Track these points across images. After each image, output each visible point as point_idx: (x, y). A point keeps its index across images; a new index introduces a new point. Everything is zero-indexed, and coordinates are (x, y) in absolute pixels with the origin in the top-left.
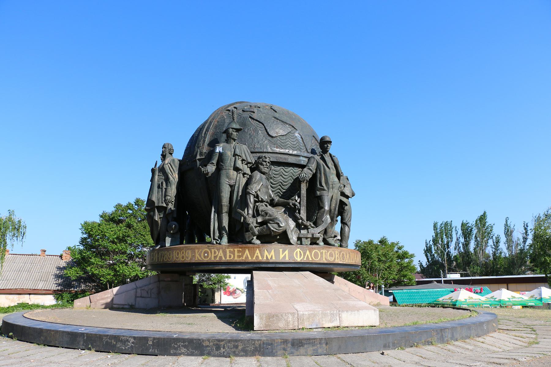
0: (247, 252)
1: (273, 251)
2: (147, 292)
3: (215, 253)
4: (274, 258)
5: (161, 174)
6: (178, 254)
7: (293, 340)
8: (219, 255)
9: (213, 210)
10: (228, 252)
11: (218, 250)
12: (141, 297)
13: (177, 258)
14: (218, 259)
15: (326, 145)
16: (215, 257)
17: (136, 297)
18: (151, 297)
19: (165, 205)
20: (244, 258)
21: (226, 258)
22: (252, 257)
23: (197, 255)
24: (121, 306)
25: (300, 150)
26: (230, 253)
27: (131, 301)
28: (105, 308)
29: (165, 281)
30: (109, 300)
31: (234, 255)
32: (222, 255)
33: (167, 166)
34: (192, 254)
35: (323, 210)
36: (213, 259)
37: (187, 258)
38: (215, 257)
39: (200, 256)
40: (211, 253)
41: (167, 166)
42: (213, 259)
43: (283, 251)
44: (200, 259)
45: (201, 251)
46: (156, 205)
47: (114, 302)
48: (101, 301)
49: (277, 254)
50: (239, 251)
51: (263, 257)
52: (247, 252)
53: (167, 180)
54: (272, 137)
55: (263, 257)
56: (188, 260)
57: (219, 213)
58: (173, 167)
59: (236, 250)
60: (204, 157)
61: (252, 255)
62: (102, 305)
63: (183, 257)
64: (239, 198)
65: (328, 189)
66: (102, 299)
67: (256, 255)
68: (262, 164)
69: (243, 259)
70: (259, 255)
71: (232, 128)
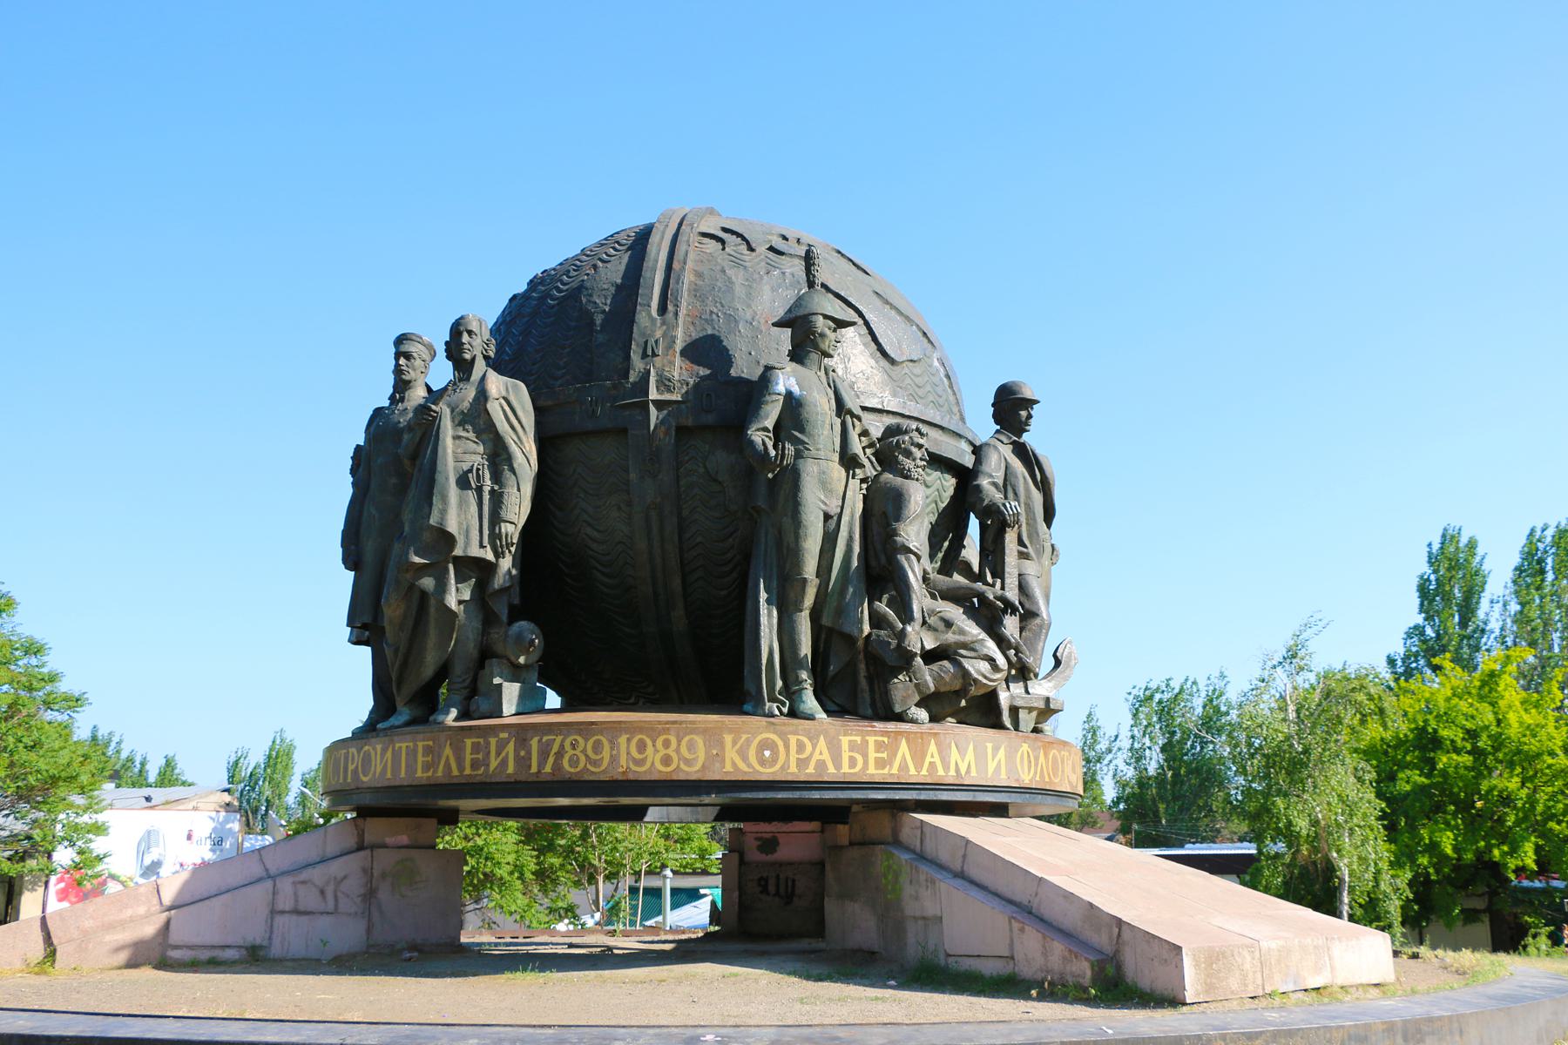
0: (904, 747)
1: (971, 747)
2: (322, 892)
3: (801, 747)
4: (974, 773)
5: (471, 435)
6: (642, 747)
7: (1405, 1022)
8: (816, 756)
9: (763, 596)
10: (845, 746)
11: (814, 740)
12: (297, 912)
14: (811, 770)
15: (1024, 413)
16: (802, 763)
17: (274, 912)
18: (335, 912)
19: (490, 556)
20: (895, 771)
21: (838, 766)
22: (919, 767)
23: (731, 754)
24: (205, 955)
25: (938, 406)
26: (851, 750)
27: (254, 933)
28: (132, 964)
29: (385, 846)
30: (149, 930)
31: (865, 756)
32: (826, 756)
33: (496, 404)
34: (708, 748)
35: (1038, 621)
36: (793, 768)
37: (688, 762)
38: (802, 763)
39: (745, 759)
40: (787, 747)
41: (496, 404)
42: (793, 768)
43: (996, 749)
44: (742, 766)
45: (748, 742)
46: (458, 552)
47: (175, 937)
48: (108, 938)
49: (981, 757)
50: (880, 747)
51: (946, 767)
52: (904, 747)
53: (499, 457)
54: (892, 362)
55: (946, 767)
58: (520, 413)
59: (871, 740)
60: (677, 397)
61: (919, 756)
62: (118, 949)
63: (666, 760)
64: (855, 563)
66: (110, 927)
67: (928, 759)
68: (908, 454)
69: (890, 773)
71: (826, 317)
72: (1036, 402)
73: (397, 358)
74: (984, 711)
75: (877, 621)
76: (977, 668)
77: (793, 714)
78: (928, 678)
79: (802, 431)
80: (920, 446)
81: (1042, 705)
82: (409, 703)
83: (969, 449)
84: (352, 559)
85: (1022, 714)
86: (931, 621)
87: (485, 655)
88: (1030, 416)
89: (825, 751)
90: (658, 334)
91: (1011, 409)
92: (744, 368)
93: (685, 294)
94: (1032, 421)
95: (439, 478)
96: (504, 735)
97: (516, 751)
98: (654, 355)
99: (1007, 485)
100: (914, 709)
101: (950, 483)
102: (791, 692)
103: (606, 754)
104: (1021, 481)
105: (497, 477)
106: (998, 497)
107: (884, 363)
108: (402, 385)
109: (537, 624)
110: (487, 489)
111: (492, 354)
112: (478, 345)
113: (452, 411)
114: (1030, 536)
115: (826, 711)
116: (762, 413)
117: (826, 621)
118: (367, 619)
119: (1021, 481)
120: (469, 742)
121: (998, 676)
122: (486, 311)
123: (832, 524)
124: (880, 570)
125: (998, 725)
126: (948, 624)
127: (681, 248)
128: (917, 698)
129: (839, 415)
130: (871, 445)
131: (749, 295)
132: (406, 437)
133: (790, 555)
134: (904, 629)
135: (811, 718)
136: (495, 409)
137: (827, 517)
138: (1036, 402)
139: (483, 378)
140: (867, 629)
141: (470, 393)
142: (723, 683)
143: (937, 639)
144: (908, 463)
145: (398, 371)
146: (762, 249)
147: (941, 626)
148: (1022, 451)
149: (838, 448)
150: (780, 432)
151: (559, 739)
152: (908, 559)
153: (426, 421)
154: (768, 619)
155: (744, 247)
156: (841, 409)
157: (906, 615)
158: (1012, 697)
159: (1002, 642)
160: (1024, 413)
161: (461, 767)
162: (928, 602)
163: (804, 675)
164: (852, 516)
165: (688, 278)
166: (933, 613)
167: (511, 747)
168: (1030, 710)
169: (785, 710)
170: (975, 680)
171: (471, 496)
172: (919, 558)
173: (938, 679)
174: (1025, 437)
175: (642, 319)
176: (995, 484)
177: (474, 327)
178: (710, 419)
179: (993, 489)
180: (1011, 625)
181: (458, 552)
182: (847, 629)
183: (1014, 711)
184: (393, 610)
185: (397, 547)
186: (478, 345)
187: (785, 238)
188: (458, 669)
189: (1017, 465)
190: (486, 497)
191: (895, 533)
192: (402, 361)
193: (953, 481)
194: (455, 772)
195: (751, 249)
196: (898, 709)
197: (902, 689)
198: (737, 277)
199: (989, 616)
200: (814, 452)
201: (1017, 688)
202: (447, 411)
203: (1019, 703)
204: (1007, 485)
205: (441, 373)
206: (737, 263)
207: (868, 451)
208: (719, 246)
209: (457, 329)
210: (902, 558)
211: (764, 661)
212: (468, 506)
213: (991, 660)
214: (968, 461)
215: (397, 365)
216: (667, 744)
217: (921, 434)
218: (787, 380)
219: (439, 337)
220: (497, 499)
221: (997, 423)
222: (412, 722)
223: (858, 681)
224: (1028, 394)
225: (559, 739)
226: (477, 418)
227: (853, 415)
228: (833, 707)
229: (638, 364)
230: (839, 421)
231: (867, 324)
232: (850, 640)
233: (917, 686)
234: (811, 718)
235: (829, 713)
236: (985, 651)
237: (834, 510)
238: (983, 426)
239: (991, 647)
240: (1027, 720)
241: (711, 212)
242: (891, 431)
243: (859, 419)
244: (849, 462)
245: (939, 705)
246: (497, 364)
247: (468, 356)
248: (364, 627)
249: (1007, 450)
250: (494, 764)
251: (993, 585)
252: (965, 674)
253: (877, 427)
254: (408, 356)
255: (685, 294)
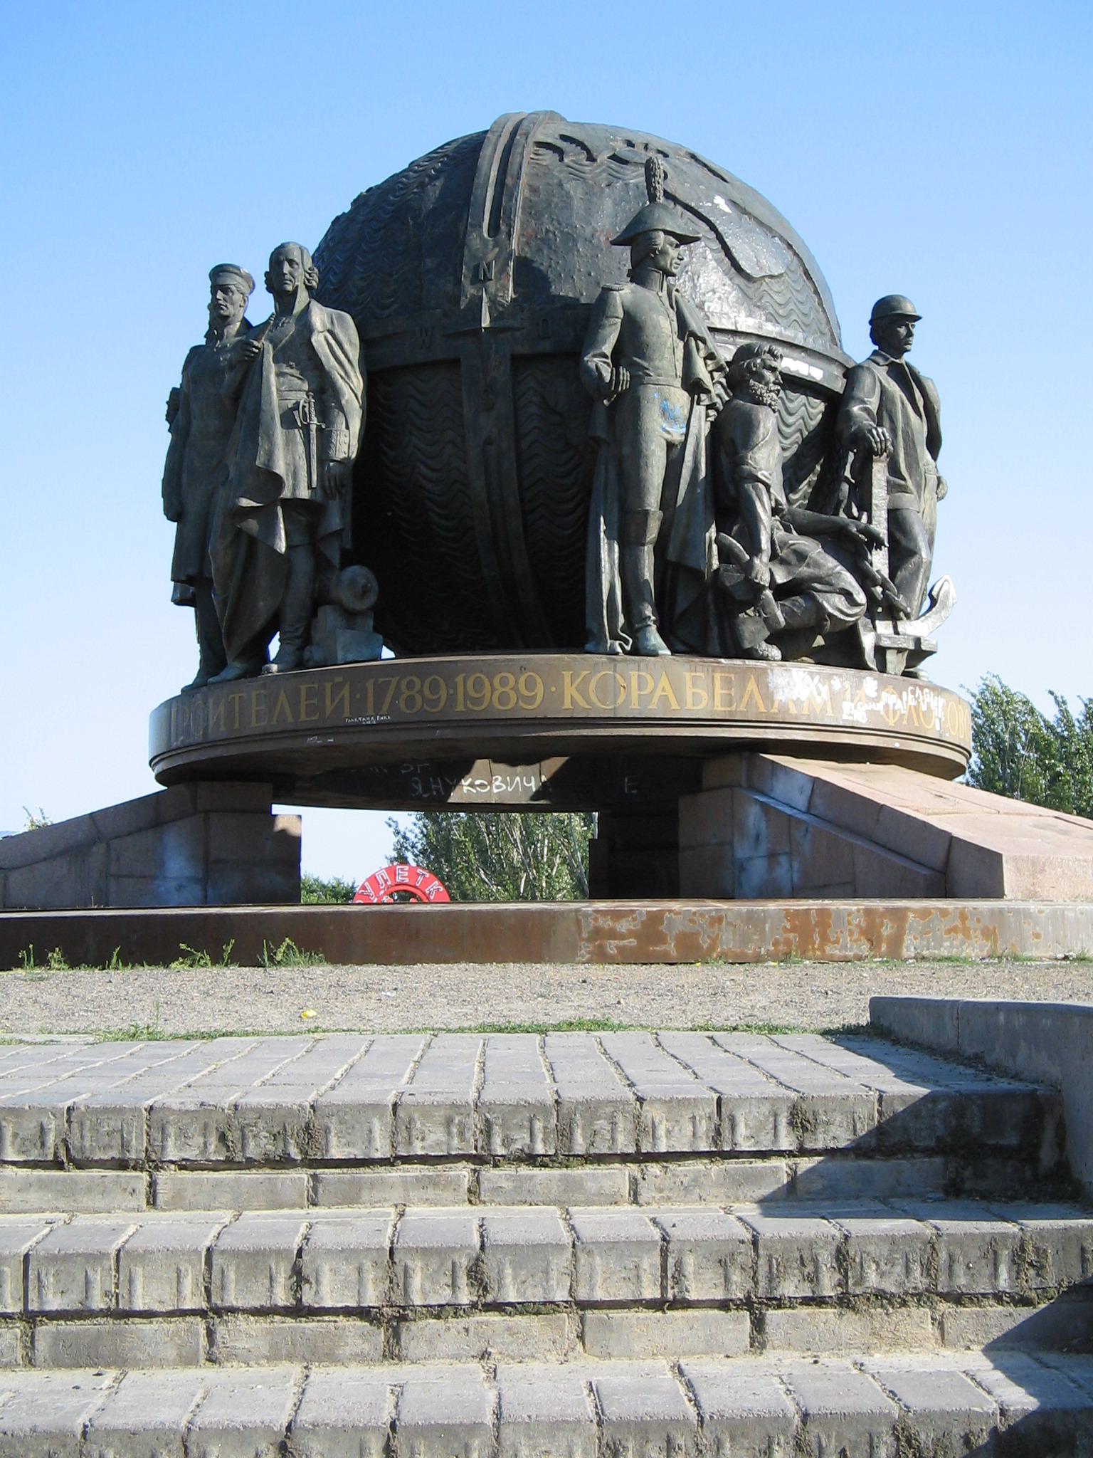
8: (659, 693)
13: (478, 701)
15: (903, 331)
23: (570, 691)
25: (805, 327)
35: (915, 559)
45: (586, 680)
46: (287, 493)
50: (728, 683)
53: (325, 393)
54: (748, 278)
56: (532, 709)
57: (628, 542)
58: (347, 347)
65: (918, 487)
68: (760, 378)
70: (757, 697)
71: (667, 232)
72: (917, 318)
73: (214, 292)
74: (843, 650)
75: (726, 555)
76: (833, 604)
77: (635, 651)
78: (779, 613)
79: (643, 357)
80: (773, 369)
81: (912, 646)
82: (238, 657)
83: (838, 372)
84: (174, 510)
85: (890, 656)
86: (782, 553)
87: (318, 600)
88: (910, 334)
89: (668, 687)
90: (491, 256)
91: (890, 324)
92: (573, 286)
93: (519, 212)
94: (914, 340)
95: (265, 418)
96: (339, 679)
97: (352, 696)
98: (487, 279)
99: (885, 411)
100: (764, 645)
101: (818, 407)
102: (634, 627)
103: (443, 693)
104: (899, 405)
105: (324, 414)
106: (868, 422)
107: (740, 280)
108: (218, 319)
109: (371, 568)
110: (313, 428)
111: (314, 284)
112: (300, 277)
113: (274, 348)
114: (909, 467)
115: (670, 647)
116: (600, 338)
117: (672, 555)
118: (192, 571)
119: (899, 405)
120: (303, 688)
121: (857, 610)
122: (308, 235)
123: (676, 452)
124: (726, 492)
125: (861, 665)
126: (801, 556)
127: (514, 160)
128: (767, 634)
129: (681, 337)
130: (719, 369)
131: (588, 211)
132: (227, 377)
133: (630, 483)
134: (751, 562)
135: (654, 654)
136: (319, 341)
137: (670, 446)
138: (917, 318)
139: (307, 310)
140: (715, 563)
141: (290, 328)
142: (566, 624)
143: (789, 573)
144: (760, 388)
145: (215, 307)
146: (603, 157)
147: (793, 559)
148: (907, 378)
149: (680, 373)
150: (618, 357)
151: (394, 681)
152: (755, 488)
153: (249, 365)
154: (608, 556)
155: (584, 155)
156: (684, 330)
157: (755, 549)
158: (878, 637)
159: (866, 579)
160: (903, 331)
161: (296, 714)
162: (780, 534)
163: (648, 611)
164: (698, 444)
165: (522, 194)
166: (784, 544)
167: (346, 691)
168: (900, 650)
169: (628, 648)
170: (830, 615)
171: (298, 435)
172: (768, 487)
173: (788, 614)
174: (906, 358)
175: (474, 241)
176: (868, 411)
177: (296, 256)
178: (546, 346)
179: (865, 415)
180: (879, 561)
181: (287, 493)
182: (691, 563)
183: (880, 651)
184: (219, 555)
185: (222, 493)
186: (300, 277)
187: (630, 144)
188: (290, 616)
189: (894, 388)
190: (313, 433)
191: (743, 461)
192: (220, 295)
193: (822, 407)
194: (290, 719)
195: (591, 158)
196: (747, 645)
197: (751, 628)
198: (575, 189)
199: (853, 550)
200: (654, 378)
201: (884, 627)
202: (269, 348)
203: (885, 643)
204: (885, 411)
205: (260, 307)
206: (577, 175)
207: (716, 375)
208: (556, 157)
209: (279, 258)
210: (749, 487)
211: (605, 598)
212: (295, 443)
213: (848, 595)
214: (839, 386)
215: (214, 299)
216: (504, 682)
217: (775, 356)
218: (625, 293)
219: (258, 268)
220: (325, 438)
221: (875, 342)
222: (244, 675)
223: (703, 617)
224: (909, 309)
225: (394, 681)
226: (301, 354)
227: (697, 338)
228: (680, 647)
229: (471, 290)
230: (681, 344)
231: (720, 237)
232: (697, 574)
233: (765, 620)
234: (654, 654)
235: (674, 652)
236: (842, 585)
237: (677, 437)
238: (859, 346)
239: (848, 580)
240: (895, 662)
241: (552, 116)
242: (744, 353)
243: (704, 341)
244: (694, 387)
245: (792, 643)
246: (319, 295)
247: (290, 288)
248: (190, 581)
249: (881, 372)
250: (329, 708)
251: (859, 519)
252: (820, 608)
253: (726, 353)
254: (225, 290)
255: (519, 212)
